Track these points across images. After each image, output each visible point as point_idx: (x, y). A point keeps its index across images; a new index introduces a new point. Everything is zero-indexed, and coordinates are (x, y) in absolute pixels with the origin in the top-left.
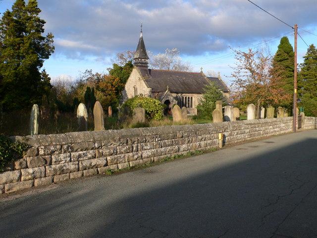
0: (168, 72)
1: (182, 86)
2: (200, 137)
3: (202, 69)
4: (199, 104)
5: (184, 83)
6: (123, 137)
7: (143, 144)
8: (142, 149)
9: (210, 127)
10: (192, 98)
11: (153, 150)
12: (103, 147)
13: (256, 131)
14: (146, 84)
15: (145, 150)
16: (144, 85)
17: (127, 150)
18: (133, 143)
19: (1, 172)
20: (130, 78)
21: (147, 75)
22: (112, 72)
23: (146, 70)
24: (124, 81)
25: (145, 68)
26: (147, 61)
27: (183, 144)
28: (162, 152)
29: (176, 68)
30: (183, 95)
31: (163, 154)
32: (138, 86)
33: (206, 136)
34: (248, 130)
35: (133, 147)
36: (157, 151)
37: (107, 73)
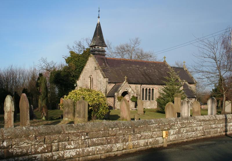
0: (130, 61)
1: (142, 76)
2: (139, 135)
3: (165, 58)
4: (160, 97)
5: (145, 74)
6: (41, 134)
7: (66, 143)
8: (65, 148)
9: (152, 124)
10: (153, 89)
11: (78, 150)
12: (13, 147)
13: (212, 128)
14: (102, 74)
15: (68, 149)
16: (101, 75)
17: (44, 149)
18: (53, 142)
19: (227, 137)
20: (85, 67)
21: (104, 64)
22: (68, 61)
23: (102, 59)
24: (80, 68)
25: (102, 57)
26: (105, 48)
27: (116, 142)
28: (90, 152)
29: (138, 57)
30: (143, 86)
31: (91, 154)
32: (93, 77)
33: (147, 134)
34: (201, 128)
35: (51, 146)
36: (83, 150)
37: (65, 64)
